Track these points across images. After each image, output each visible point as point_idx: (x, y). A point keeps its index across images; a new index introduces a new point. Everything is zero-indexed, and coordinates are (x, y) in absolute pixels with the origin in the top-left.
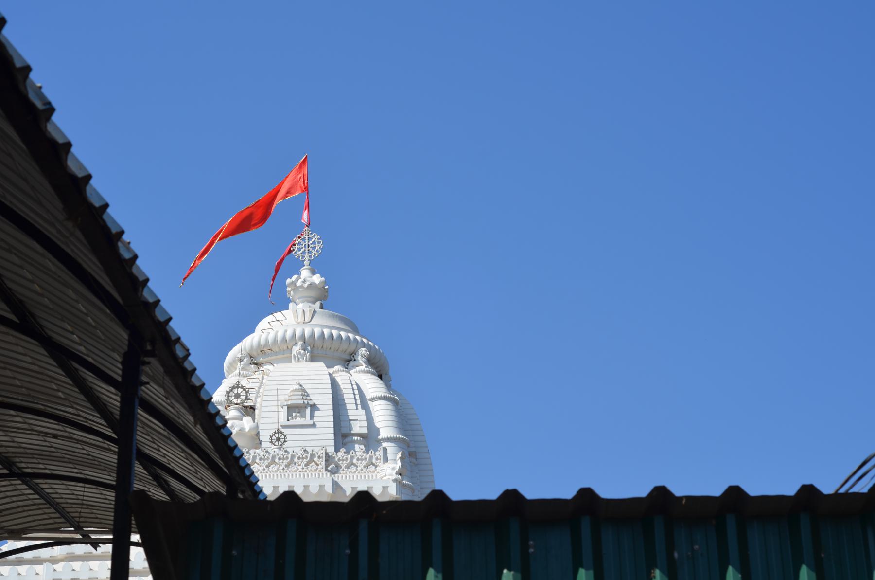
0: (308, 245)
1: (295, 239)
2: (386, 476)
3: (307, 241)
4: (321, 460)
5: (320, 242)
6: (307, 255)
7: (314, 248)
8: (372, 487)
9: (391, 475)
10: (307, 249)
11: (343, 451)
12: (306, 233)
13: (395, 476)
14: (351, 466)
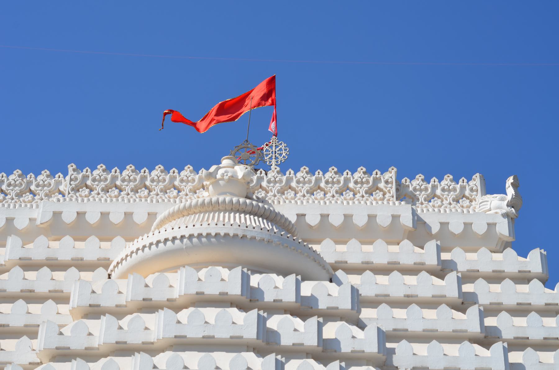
0: (275, 152)
1: (263, 146)
2: (490, 210)
3: (274, 148)
4: (390, 185)
5: (287, 149)
6: (274, 160)
7: (281, 155)
8: (472, 224)
9: (499, 208)
10: (274, 155)
11: (420, 178)
12: (273, 141)
13: (506, 209)
14: (433, 198)
